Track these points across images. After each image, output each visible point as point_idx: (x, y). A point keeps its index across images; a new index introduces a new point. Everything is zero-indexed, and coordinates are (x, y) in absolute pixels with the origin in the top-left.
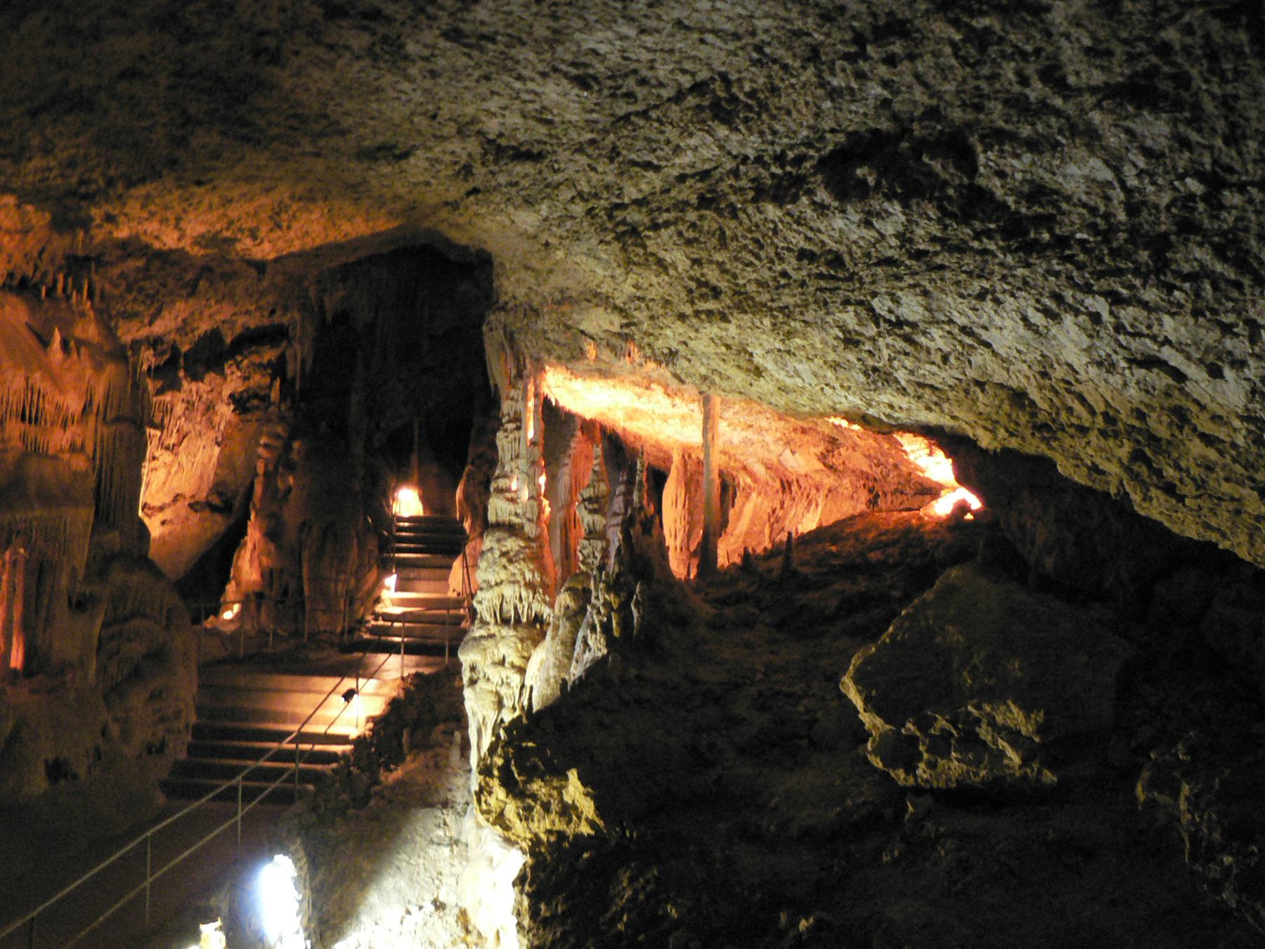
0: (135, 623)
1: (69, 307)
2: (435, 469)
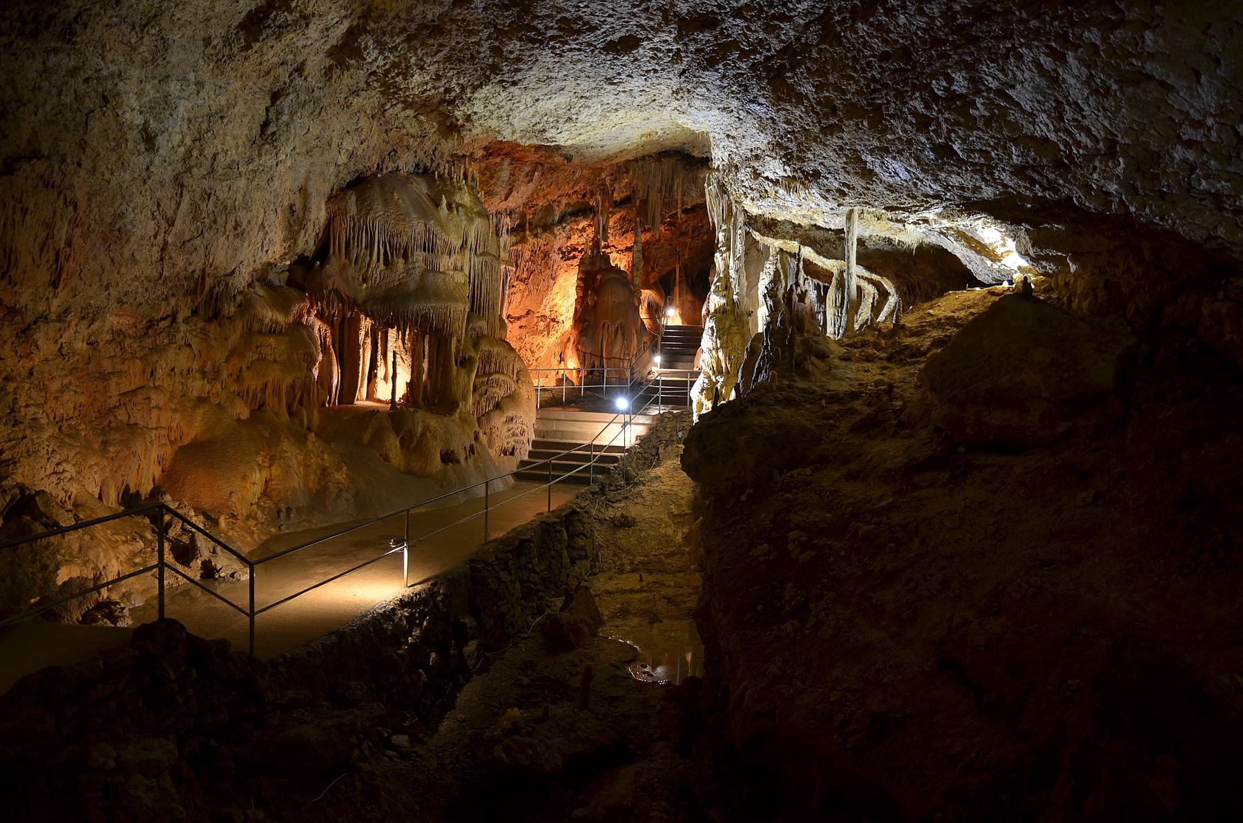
0: (496, 376)
1: (452, 183)
2: (690, 298)
